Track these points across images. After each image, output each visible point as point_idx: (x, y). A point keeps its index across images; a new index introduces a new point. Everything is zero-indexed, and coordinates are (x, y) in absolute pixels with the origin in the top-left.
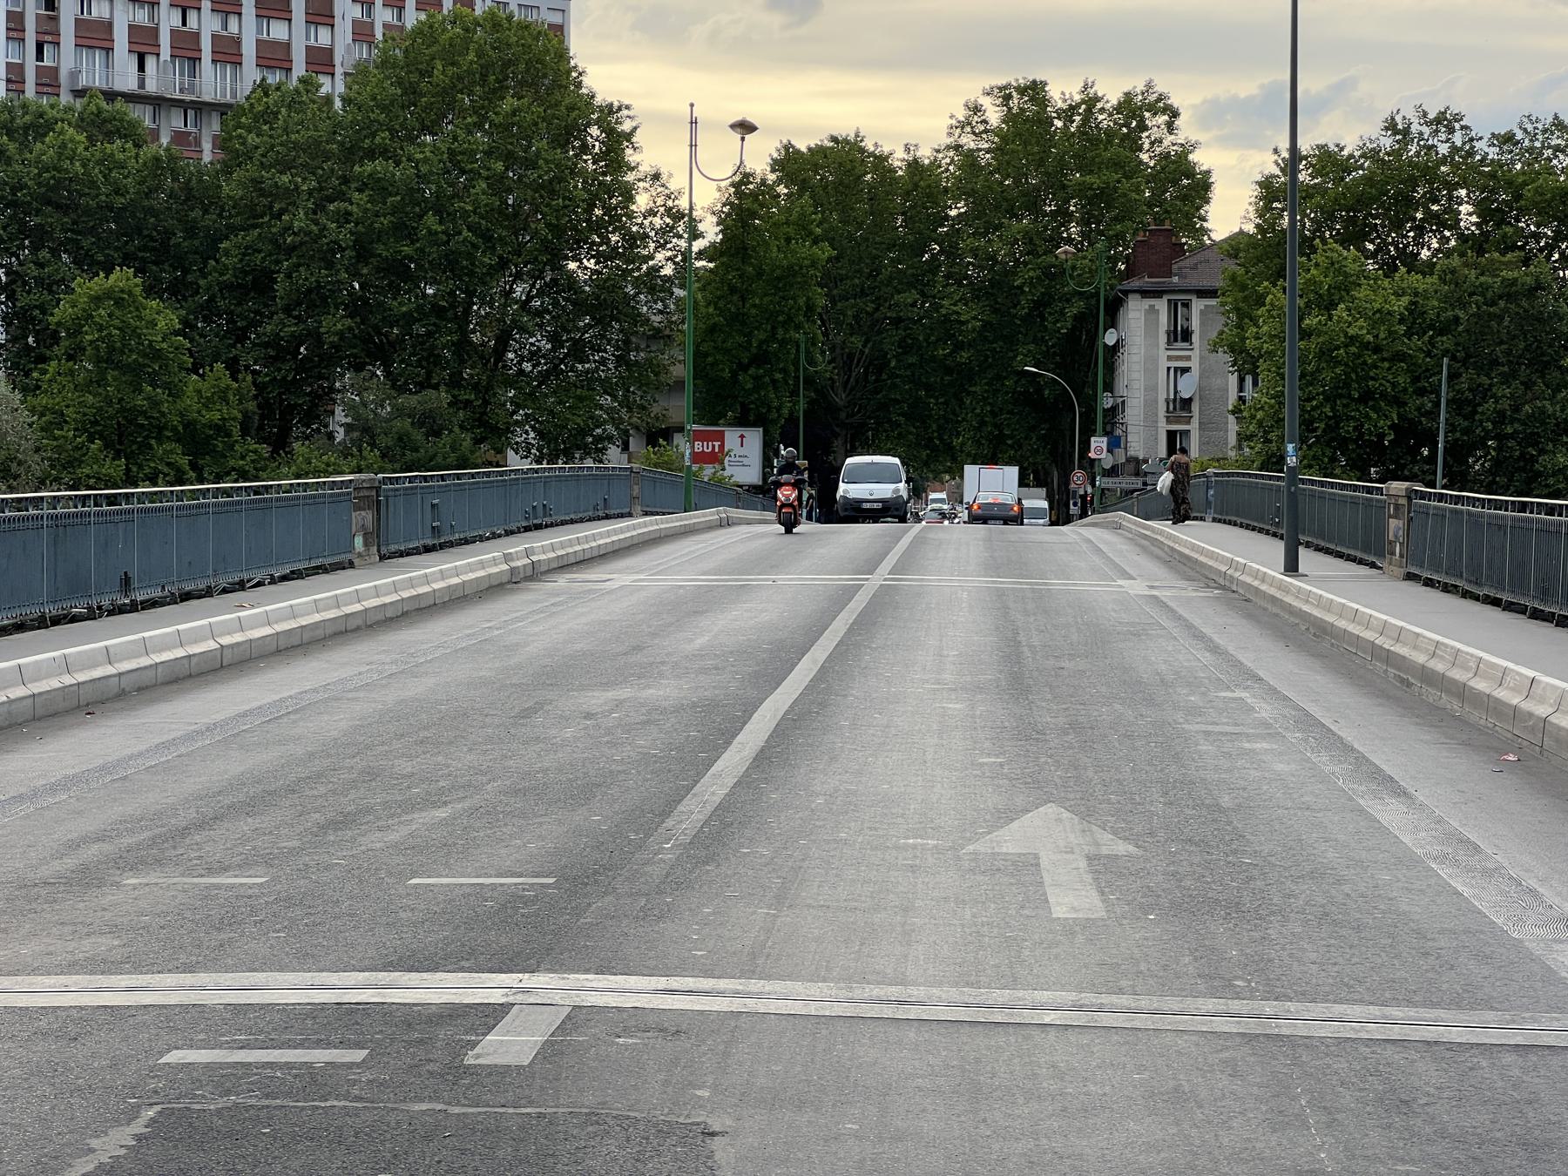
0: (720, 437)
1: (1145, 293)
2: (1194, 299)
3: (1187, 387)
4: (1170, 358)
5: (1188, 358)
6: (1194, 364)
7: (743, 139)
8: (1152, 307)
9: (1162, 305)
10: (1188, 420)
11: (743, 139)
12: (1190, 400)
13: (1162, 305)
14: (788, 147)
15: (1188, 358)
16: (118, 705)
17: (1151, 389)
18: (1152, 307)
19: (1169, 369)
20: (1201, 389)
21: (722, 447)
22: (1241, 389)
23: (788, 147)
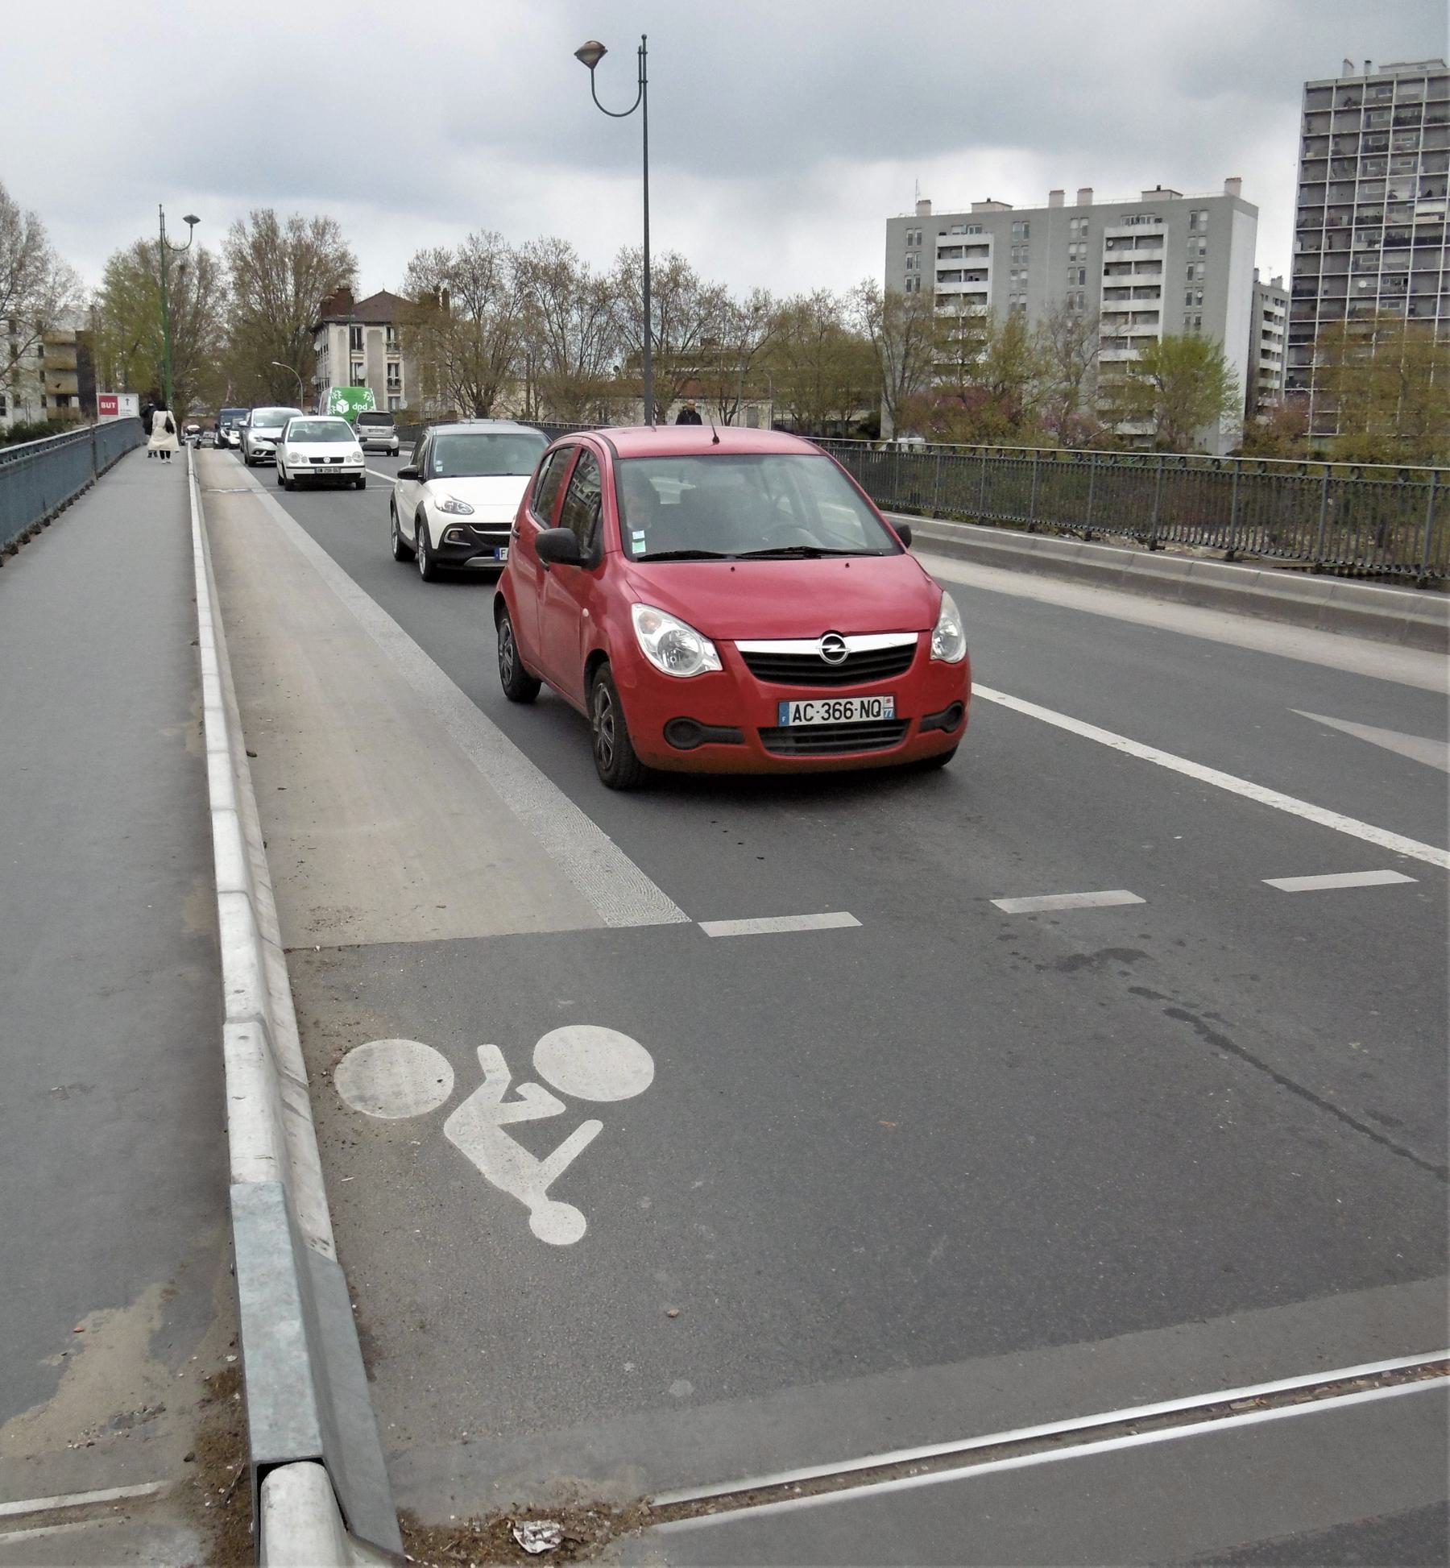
0: (114, 399)
1: (339, 323)
2: (363, 326)
3: (361, 373)
4: (389, 358)
5: (362, 358)
6: (365, 361)
7: (192, 227)
8: (342, 330)
9: (347, 329)
10: (398, 391)
11: (192, 227)
12: (364, 380)
13: (347, 329)
14: (892, 223)
15: (362, 358)
16: (232, 776)
17: (343, 374)
18: (342, 330)
19: (389, 366)
20: (369, 374)
21: (116, 406)
22: (389, 374)
23: (892, 223)
